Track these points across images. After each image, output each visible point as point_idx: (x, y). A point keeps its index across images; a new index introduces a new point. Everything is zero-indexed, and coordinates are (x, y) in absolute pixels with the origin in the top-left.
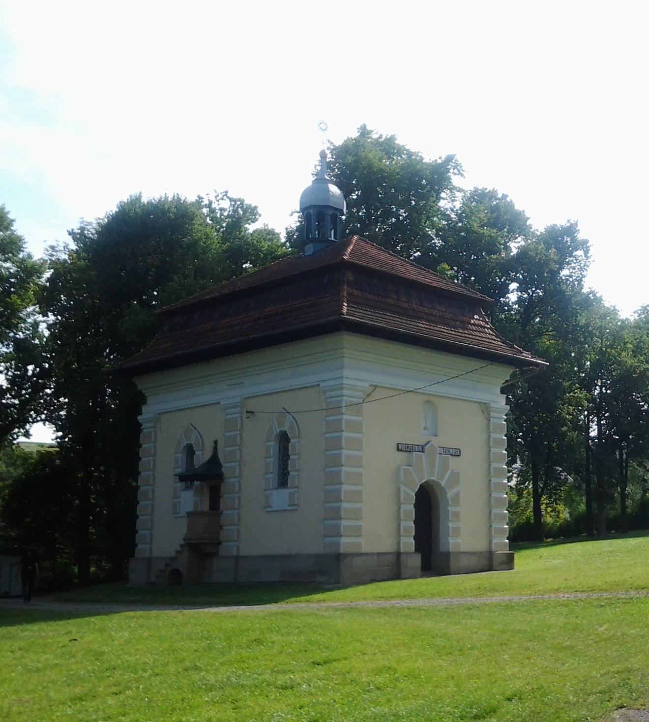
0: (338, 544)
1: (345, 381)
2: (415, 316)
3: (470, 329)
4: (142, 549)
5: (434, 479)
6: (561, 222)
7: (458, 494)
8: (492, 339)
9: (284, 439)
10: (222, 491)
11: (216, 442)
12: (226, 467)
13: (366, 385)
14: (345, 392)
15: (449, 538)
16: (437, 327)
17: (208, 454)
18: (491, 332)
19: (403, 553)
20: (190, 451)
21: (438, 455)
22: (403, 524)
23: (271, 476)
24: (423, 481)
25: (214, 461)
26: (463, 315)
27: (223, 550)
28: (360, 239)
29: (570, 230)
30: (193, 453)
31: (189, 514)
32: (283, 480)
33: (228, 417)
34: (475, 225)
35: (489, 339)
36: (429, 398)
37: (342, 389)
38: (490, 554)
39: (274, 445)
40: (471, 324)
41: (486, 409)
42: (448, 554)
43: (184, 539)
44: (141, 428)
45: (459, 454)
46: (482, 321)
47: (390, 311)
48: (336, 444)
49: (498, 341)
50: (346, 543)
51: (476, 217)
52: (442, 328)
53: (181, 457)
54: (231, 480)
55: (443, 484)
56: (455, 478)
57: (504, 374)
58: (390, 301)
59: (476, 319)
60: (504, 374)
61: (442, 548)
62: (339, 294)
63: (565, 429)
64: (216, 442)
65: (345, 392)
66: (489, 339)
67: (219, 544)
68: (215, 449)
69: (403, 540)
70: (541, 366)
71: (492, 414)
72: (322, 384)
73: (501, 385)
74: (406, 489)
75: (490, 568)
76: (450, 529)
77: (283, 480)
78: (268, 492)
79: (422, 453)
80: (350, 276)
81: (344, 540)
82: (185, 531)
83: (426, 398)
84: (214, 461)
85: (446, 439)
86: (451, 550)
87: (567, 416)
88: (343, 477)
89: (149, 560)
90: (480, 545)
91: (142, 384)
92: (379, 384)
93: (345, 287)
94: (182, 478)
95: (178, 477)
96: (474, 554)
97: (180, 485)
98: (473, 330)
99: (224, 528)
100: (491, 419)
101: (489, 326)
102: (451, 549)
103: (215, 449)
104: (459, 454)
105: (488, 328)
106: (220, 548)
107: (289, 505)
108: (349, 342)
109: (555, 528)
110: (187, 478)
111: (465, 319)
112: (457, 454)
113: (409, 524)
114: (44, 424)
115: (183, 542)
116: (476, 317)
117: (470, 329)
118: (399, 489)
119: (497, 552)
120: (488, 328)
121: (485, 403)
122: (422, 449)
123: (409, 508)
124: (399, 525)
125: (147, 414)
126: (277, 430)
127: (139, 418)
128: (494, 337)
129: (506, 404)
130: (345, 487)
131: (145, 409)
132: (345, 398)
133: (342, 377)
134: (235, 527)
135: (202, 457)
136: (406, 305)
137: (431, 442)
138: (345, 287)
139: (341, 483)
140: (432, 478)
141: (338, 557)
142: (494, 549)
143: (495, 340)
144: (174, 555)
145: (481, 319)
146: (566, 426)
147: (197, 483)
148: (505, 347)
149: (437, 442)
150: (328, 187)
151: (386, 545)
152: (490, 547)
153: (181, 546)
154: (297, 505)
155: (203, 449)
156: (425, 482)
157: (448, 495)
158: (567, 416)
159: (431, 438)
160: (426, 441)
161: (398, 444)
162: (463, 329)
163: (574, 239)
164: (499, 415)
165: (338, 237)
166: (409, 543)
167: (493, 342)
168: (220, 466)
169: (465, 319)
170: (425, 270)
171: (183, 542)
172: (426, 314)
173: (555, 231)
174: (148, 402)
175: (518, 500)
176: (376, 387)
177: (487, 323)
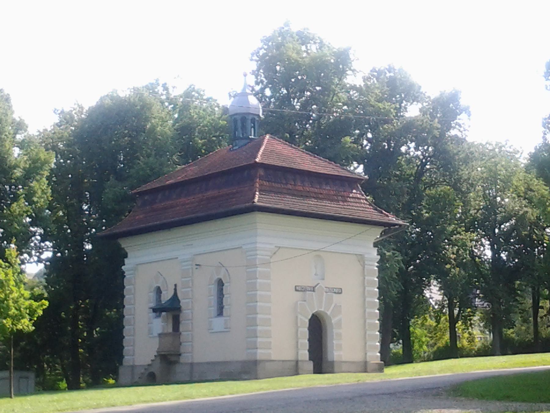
0: (256, 353)
1: (258, 245)
2: (306, 196)
3: (349, 202)
4: (127, 359)
5: (322, 310)
6: (448, 90)
7: (340, 320)
8: (366, 208)
9: (220, 283)
10: (181, 319)
11: (176, 285)
12: (183, 303)
13: (273, 247)
14: (258, 252)
15: (334, 352)
16: (323, 202)
17: (170, 294)
18: (366, 202)
19: (301, 361)
20: (159, 291)
21: (325, 293)
22: (300, 341)
23: (213, 308)
24: (314, 312)
25: (175, 298)
26: (344, 191)
27: (182, 360)
28: (272, 138)
29: (454, 97)
30: (161, 293)
31: (160, 335)
32: (220, 312)
33: (183, 268)
34: (373, 100)
35: (363, 207)
36: (317, 253)
37: (256, 250)
38: (366, 363)
39: (214, 288)
40: (350, 197)
41: (361, 259)
42: (332, 363)
43: (158, 352)
44: (125, 274)
45: (340, 291)
46: (359, 194)
47: (289, 194)
48: (253, 287)
49: (370, 209)
50: (261, 354)
51: (372, 93)
52: (327, 203)
53: (153, 295)
54: (187, 311)
55: (329, 313)
56: (338, 309)
57: (376, 233)
58: (290, 187)
59: (354, 193)
60: (376, 233)
61: (330, 359)
62: (253, 186)
63: (448, 266)
64: (176, 285)
65: (258, 252)
66: (363, 207)
67: (180, 355)
68: (175, 290)
69: (300, 352)
70: (403, 226)
71: (366, 262)
72: (244, 247)
73: (373, 241)
74: (302, 318)
75: (366, 371)
76: (335, 345)
77: (220, 312)
78: (210, 320)
79: (313, 292)
80: (261, 172)
81: (259, 351)
82: (157, 347)
83: (315, 253)
84: (175, 298)
85: (331, 282)
86: (335, 360)
87: (451, 256)
88: (258, 310)
89: (133, 367)
90: (358, 357)
91: (125, 244)
92: (282, 246)
93: (258, 180)
94: (155, 310)
95: (152, 310)
96: (353, 363)
97: (153, 315)
98: (351, 202)
99: (183, 344)
100: (366, 266)
101: (364, 198)
102: (336, 359)
103: (175, 290)
104: (340, 291)
105: (363, 199)
106: (181, 357)
107: (225, 328)
108: (259, 217)
109: (473, 352)
110: (158, 310)
111: (345, 194)
112: (340, 291)
113: (305, 342)
114: (37, 264)
115: (156, 354)
116: (354, 191)
117: (349, 202)
118: (297, 317)
119: (372, 362)
120: (363, 199)
121: (361, 255)
122: (313, 289)
123: (304, 331)
124: (297, 342)
125: (128, 265)
126: (216, 277)
127: (123, 267)
128: (368, 206)
129: (378, 255)
130: (259, 316)
131: (126, 260)
132: (258, 256)
133: (256, 243)
134: (190, 343)
135: (167, 296)
136: (301, 188)
137: (319, 285)
138: (258, 180)
139: (257, 314)
140: (320, 310)
141: (255, 363)
142: (368, 360)
143: (368, 208)
144: (150, 363)
145: (359, 192)
146: (450, 264)
147: (164, 313)
148: (376, 213)
149: (323, 284)
150: (248, 99)
151: (288, 355)
152: (366, 358)
153: (155, 356)
154: (230, 328)
155: (167, 290)
156: (316, 312)
157: (333, 321)
158: (451, 256)
159: (320, 281)
160: (316, 284)
161: (296, 286)
162: (343, 201)
163: (457, 105)
164: (371, 263)
165: (256, 134)
166: (304, 354)
167: (367, 209)
168: (179, 302)
169: (345, 194)
170: (317, 158)
171: (156, 354)
172: (315, 193)
173: (442, 98)
174: (129, 255)
175: (437, 326)
176: (280, 247)
177: (363, 195)
